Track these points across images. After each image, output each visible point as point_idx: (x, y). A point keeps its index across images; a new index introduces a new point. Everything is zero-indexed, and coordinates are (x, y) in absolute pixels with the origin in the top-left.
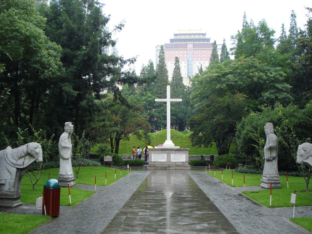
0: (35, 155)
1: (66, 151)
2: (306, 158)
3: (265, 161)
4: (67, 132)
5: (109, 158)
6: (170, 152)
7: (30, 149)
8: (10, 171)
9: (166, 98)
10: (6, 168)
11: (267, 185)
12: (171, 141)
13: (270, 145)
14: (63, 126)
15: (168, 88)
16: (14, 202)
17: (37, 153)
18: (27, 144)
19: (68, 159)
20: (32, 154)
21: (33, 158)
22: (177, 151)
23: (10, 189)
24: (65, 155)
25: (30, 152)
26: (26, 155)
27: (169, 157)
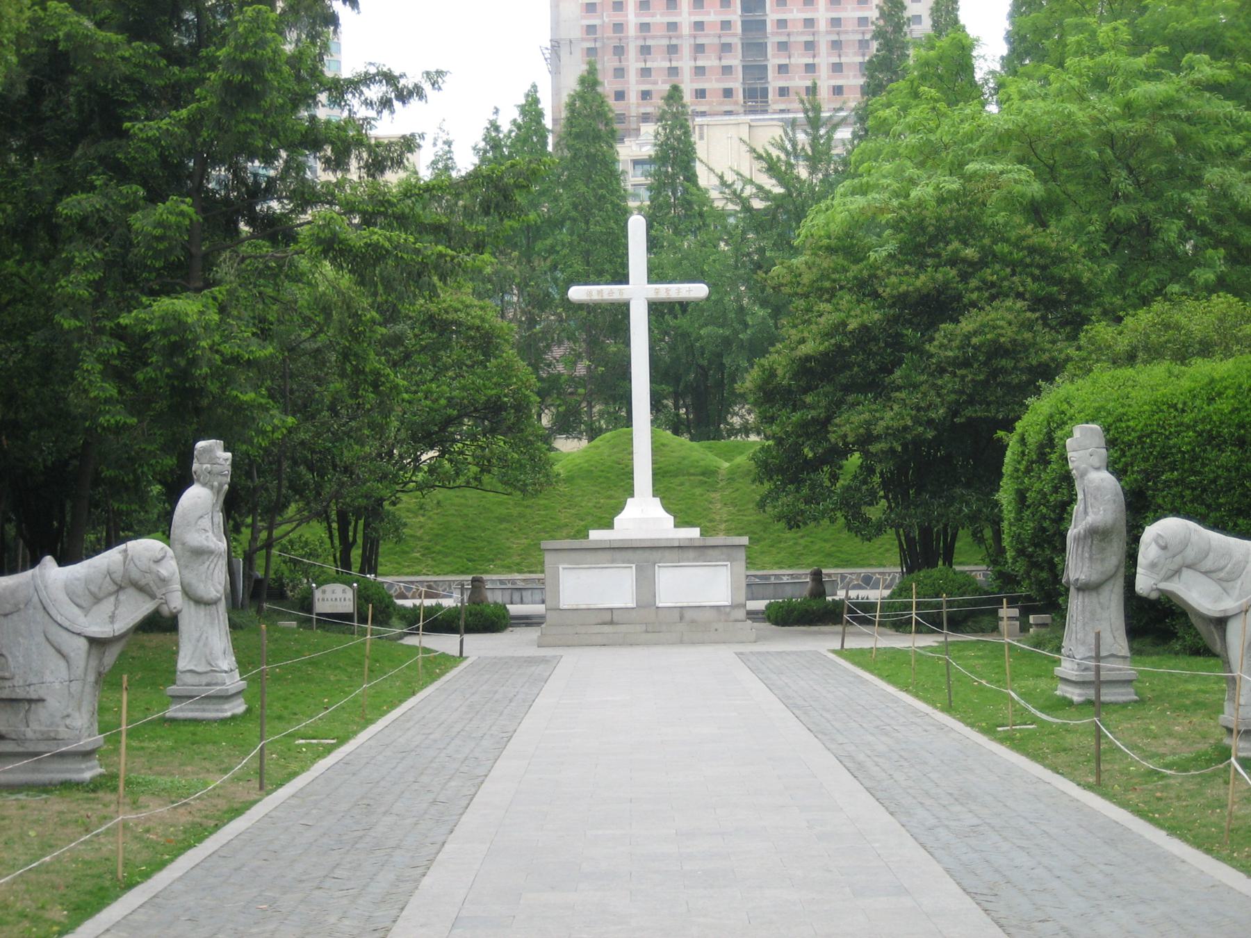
0: (154, 588)
1: (206, 565)
2: (1170, 573)
3: (1072, 589)
4: (204, 485)
5: (339, 594)
6: (656, 555)
7: (138, 563)
8: (65, 649)
9: (627, 282)
10: (48, 639)
11: (1077, 691)
12: (658, 499)
13: (1090, 519)
14: (187, 457)
15: (637, 227)
16: (83, 766)
17: (164, 581)
18: (122, 547)
19: (214, 602)
20: (143, 582)
21: (148, 598)
22: (691, 554)
23: (68, 716)
24: (202, 586)
25: (135, 574)
26: (120, 588)
27: (646, 584)
